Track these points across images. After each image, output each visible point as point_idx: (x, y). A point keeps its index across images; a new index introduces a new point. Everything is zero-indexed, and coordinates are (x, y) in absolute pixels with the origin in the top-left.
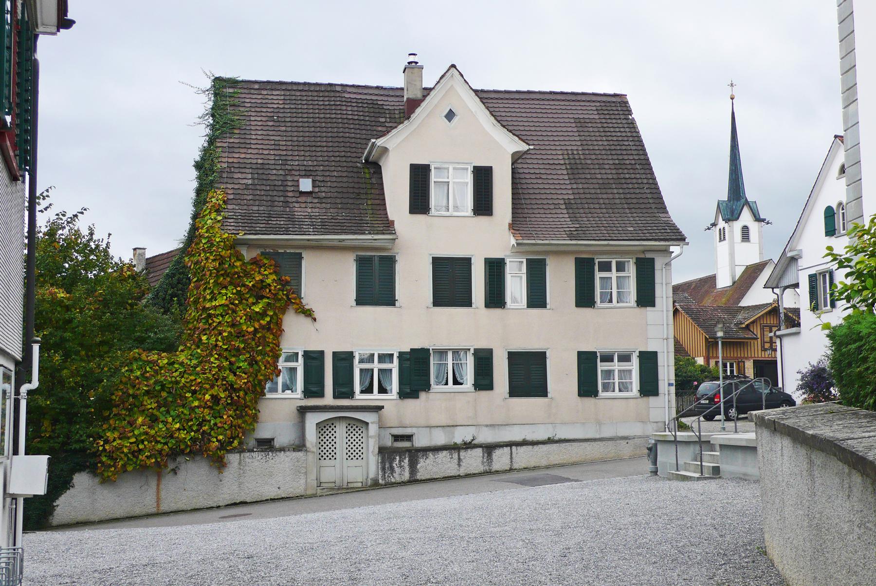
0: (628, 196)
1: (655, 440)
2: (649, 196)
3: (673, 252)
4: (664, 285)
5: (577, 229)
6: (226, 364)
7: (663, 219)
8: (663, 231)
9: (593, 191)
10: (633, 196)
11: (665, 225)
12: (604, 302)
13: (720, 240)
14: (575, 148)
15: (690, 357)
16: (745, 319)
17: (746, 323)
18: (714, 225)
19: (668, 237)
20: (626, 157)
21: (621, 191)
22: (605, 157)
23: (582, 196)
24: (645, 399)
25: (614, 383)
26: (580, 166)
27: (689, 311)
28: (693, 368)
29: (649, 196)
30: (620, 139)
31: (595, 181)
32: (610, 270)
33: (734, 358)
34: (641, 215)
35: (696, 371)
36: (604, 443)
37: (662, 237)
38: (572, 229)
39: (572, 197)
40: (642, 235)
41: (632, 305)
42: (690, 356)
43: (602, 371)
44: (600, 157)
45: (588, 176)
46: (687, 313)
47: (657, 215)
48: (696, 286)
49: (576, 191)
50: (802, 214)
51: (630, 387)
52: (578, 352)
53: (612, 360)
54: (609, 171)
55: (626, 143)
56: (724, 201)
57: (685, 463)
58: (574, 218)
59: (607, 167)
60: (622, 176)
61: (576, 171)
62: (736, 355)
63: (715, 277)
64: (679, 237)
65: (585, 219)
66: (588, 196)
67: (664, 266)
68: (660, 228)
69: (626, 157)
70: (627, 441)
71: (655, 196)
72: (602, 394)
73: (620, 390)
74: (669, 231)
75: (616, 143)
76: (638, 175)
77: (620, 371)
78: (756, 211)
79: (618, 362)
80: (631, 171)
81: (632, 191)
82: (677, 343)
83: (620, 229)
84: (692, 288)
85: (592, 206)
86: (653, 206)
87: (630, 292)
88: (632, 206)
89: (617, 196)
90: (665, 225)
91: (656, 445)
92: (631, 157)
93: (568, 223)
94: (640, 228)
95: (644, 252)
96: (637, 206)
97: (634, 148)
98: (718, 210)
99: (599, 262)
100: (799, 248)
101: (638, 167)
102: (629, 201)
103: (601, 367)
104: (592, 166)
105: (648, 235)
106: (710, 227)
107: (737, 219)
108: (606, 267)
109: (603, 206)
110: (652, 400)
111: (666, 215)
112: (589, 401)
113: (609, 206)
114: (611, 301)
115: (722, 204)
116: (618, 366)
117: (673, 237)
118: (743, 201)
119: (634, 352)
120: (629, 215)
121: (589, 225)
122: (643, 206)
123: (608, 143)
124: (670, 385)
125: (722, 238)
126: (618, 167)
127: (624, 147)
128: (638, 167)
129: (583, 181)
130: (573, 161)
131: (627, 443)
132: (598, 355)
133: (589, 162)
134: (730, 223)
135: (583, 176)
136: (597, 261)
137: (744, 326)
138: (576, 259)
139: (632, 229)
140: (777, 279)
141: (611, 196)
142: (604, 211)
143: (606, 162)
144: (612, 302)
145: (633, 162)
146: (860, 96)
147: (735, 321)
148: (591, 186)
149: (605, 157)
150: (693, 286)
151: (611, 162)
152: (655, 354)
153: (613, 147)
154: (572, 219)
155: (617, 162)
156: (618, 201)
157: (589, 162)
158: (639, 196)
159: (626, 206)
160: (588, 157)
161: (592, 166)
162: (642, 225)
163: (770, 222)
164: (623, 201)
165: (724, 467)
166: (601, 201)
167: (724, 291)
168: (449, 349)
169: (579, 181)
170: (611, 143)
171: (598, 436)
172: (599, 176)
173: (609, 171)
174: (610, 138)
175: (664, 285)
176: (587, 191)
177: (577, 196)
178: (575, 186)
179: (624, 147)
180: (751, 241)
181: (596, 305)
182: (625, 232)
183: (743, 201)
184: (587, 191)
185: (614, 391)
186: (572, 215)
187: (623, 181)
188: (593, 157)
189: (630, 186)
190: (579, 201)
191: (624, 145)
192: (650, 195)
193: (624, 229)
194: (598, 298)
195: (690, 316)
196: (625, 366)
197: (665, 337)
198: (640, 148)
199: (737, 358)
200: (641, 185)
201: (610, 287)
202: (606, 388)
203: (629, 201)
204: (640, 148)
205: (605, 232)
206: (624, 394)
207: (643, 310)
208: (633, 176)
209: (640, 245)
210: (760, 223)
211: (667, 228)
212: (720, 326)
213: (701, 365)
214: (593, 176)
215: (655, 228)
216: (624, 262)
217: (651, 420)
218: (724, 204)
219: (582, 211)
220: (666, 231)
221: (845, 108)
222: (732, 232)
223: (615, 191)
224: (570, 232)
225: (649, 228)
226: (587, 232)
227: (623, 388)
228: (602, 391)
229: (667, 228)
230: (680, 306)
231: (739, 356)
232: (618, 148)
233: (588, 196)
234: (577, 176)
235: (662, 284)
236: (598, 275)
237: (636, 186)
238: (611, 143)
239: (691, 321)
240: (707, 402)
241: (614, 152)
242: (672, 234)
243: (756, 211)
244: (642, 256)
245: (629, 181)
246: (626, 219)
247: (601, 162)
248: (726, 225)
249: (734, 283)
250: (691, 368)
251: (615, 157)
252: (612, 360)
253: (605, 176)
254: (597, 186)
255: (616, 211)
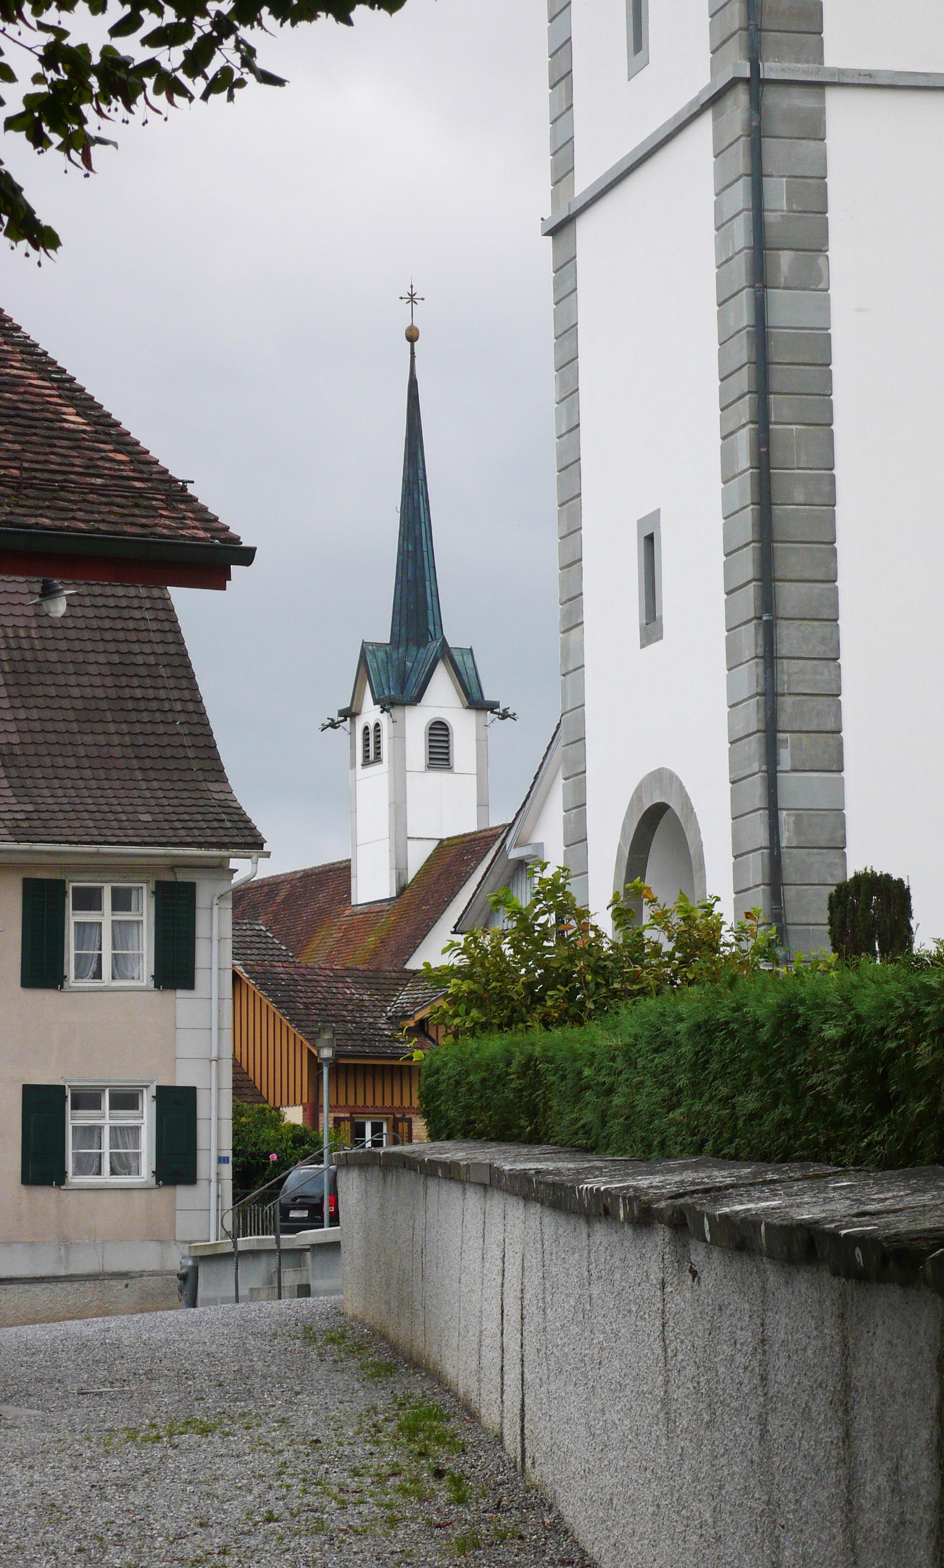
0: (141, 740)
1: (195, 1258)
2: (187, 741)
3: (236, 870)
4: (215, 943)
5: (29, 815)
6: (682, 1080)
7: (216, 796)
8: (216, 824)
9: (62, 727)
10: (152, 740)
11: (220, 810)
12: (82, 978)
13: (367, 762)
14: (21, 622)
15: (266, 1106)
16: (415, 1004)
17: (418, 1017)
18: (350, 714)
19: (226, 840)
20: (136, 648)
21: (125, 728)
22: (89, 646)
23: (40, 738)
24: (167, 1191)
25: (100, 1156)
26: (32, 668)
27: (266, 981)
28: (272, 1132)
29: (187, 741)
30: (124, 603)
31: (66, 703)
32: (98, 907)
33: (384, 1110)
34: (168, 785)
35: (281, 1140)
36: (76, 1285)
37: (214, 840)
38: (18, 816)
39: (15, 739)
40: (171, 832)
41: (144, 984)
42: (267, 1102)
43: (75, 1128)
44: (77, 645)
45: (52, 691)
46: (263, 986)
47: (204, 786)
48: (290, 895)
49: (25, 726)
50: (544, 758)
51: (134, 1165)
52: (24, 1086)
53: (97, 1105)
54: (97, 681)
55: (137, 614)
56: (379, 645)
57: (251, 1289)
58: (22, 790)
59: (93, 669)
60: (127, 693)
61: (24, 679)
62: (388, 1103)
63: (348, 868)
64: (250, 840)
65: (46, 792)
66: (53, 738)
67: (215, 901)
68: (211, 817)
69: (136, 648)
70: (125, 1282)
71: (201, 741)
72: (74, 1179)
73: (113, 1172)
74: (228, 824)
75: (114, 613)
76: (162, 692)
77: (113, 1129)
78: (473, 680)
79: (110, 1109)
80: (148, 682)
81: (149, 728)
82: (237, 1066)
83: (123, 817)
84: (279, 899)
85: (60, 761)
86: (195, 764)
87: (140, 956)
88: (148, 763)
89: (116, 739)
90: (220, 810)
91: (195, 1269)
92: (147, 649)
93: (7, 800)
94: (167, 817)
95: (173, 868)
96: (159, 764)
97: (154, 626)
98: (363, 670)
99: (75, 889)
100: (536, 839)
101: (162, 671)
102: (144, 752)
103: (74, 1119)
104: (59, 668)
105: (182, 832)
106: (337, 719)
107: (417, 699)
108: (89, 900)
109: (86, 762)
110: (182, 1193)
111: (220, 787)
112: (45, 1196)
113: (97, 763)
114: (98, 975)
115: (373, 653)
116: (111, 1118)
117: (238, 840)
118: (434, 646)
119: (147, 1087)
120: (143, 785)
121: (56, 808)
122: (172, 764)
123: (96, 612)
124: (221, 1160)
125: (372, 757)
126: (120, 670)
127: (131, 624)
128: (162, 671)
129: (41, 702)
130: (17, 655)
131: (127, 1286)
132: (68, 1093)
133: (53, 657)
134: (397, 712)
135: (40, 691)
136: (70, 887)
137: (412, 1023)
138: (24, 879)
139: (148, 818)
140: (484, 913)
141: (102, 740)
142: (88, 773)
143: (92, 657)
144: (100, 978)
145: (152, 660)
146: (587, 617)
147: (390, 1010)
148: (59, 715)
149: (89, 646)
150: (282, 894)
151: (102, 659)
152: (191, 1092)
153: (107, 624)
154: (17, 791)
155: (116, 658)
156: (117, 752)
157: (53, 657)
158: (165, 740)
159: (135, 763)
160: (51, 644)
161: (59, 668)
162: (170, 809)
163: (510, 712)
164: (130, 752)
165: (315, 1284)
166: (82, 751)
167: (374, 910)
168: (106, 1087)
169: (31, 702)
170: (103, 612)
171: (62, 1272)
172: (76, 692)
173: (97, 681)
174: (100, 601)
175: (215, 943)
176: (49, 726)
177: (27, 738)
178: (22, 714)
179: (131, 624)
180: (456, 770)
181: (65, 984)
182: (133, 824)
183: (434, 646)
184: (49, 726)
185: (99, 1173)
186: (16, 782)
187: (130, 705)
188: (63, 645)
189: (146, 717)
190: (31, 750)
191: (131, 618)
192: (189, 738)
193: (131, 817)
194: (70, 969)
195: (271, 993)
196: (125, 1118)
197: (214, 1055)
198: (167, 626)
199: (391, 1110)
200: (169, 715)
201: (98, 944)
202: (91, 1165)
203: (144, 752)
204: (167, 626)
205: (91, 824)
206: (122, 1180)
207: (168, 995)
208: (151, 693)
209: (165, 856)
210: (482, 714)
211: (224, 817)
212: (327, 1036)
213: (295, 1127)
214: (63, 691)
215: (199, 817)
216: (129, 891)
217: (179, 1237)
218: (381, 655)
219: (38, 773)
220: (221, 824)
221: (563, 632)
222: (400, 738)
223: (112, 728)
224: (14, 824)
225: (186, 817)
226: (52, 823)
227: (122, 1165)
228: (74, 1174)
229: (224, 817)
230: (244, 965)
231: (397, 1103)
232: (119, 624)
233: (53, 738)
234: (26, 691)
235: (210, 939)
236: (73, 918)
237: (158, 717)
238: (103, 612)
239: (272, 1007)
240: (305, 1214)
241: (108, 636)
242: (235, 832)
243: (473, 680)
244: (168, 877)
245: (142, 705)
246: (136, 793)
247: (80, 657)
248: (384, 719)
249: (402, 890)
250: (269, 1133)
251: (112, 647)
252: (97, 1105)
253: (88, 692)
254: (71, 715)
255: (114, 774)
